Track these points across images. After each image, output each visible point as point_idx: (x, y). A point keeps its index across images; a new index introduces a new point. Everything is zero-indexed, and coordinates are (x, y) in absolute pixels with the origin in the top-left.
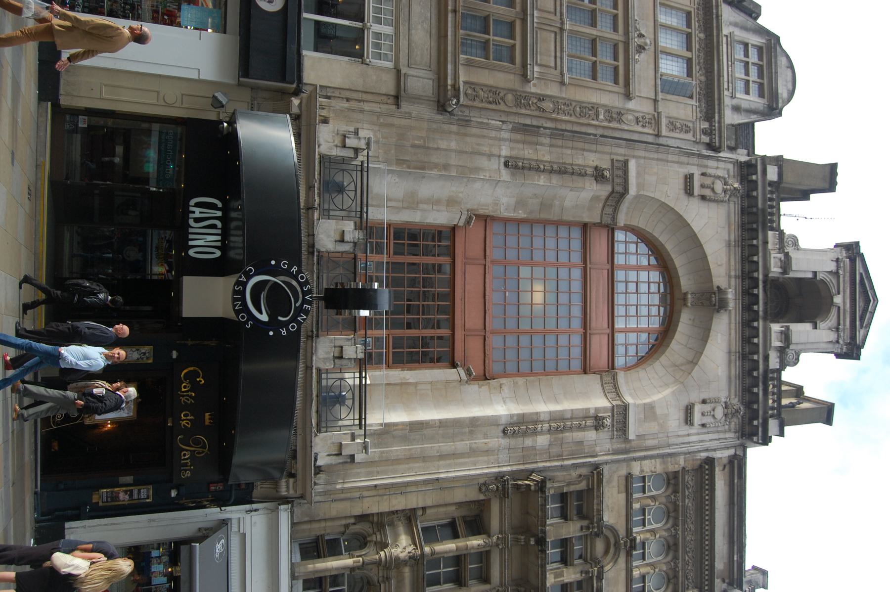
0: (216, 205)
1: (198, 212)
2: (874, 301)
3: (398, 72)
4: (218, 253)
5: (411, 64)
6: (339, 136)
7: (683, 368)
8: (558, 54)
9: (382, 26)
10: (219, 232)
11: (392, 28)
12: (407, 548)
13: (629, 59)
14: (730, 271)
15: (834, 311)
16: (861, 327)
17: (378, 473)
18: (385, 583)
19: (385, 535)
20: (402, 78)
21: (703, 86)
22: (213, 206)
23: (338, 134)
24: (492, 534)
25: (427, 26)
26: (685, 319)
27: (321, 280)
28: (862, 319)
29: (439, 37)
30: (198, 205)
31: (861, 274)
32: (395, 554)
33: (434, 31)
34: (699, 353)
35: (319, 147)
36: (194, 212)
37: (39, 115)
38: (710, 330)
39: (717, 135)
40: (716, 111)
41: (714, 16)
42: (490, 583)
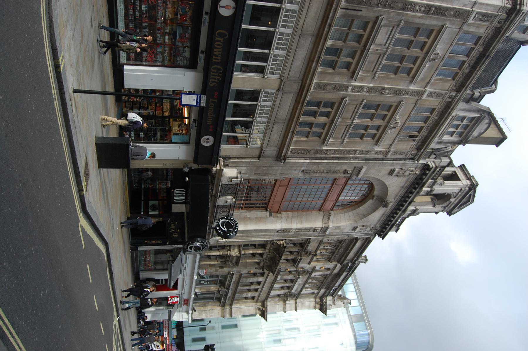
1: (177, 192)
2: (472, 202)
3: (262, 149)
4: (184, 201)
5: (303, 31)
7: (360, 216)
8: (345, 133)
11: (285, 51)
13: (384, 133)
14: (398, 194)
15: (448, 203)
16: (458, 208)
19: (231, 248)
20: (263, 152)
21: (423, 138)
22: (183, 191)
25: (279, 134)
26: (369, 203)
28: (462, 205)
29: (284, 137)
30: (177, 191)
31: (470, 195)
33: (282, 135)
34: (369, 214)
38: (377, 209)
39: (418, 156)
40: (424, 148)
41: (448, 113)
42: (262, 257)
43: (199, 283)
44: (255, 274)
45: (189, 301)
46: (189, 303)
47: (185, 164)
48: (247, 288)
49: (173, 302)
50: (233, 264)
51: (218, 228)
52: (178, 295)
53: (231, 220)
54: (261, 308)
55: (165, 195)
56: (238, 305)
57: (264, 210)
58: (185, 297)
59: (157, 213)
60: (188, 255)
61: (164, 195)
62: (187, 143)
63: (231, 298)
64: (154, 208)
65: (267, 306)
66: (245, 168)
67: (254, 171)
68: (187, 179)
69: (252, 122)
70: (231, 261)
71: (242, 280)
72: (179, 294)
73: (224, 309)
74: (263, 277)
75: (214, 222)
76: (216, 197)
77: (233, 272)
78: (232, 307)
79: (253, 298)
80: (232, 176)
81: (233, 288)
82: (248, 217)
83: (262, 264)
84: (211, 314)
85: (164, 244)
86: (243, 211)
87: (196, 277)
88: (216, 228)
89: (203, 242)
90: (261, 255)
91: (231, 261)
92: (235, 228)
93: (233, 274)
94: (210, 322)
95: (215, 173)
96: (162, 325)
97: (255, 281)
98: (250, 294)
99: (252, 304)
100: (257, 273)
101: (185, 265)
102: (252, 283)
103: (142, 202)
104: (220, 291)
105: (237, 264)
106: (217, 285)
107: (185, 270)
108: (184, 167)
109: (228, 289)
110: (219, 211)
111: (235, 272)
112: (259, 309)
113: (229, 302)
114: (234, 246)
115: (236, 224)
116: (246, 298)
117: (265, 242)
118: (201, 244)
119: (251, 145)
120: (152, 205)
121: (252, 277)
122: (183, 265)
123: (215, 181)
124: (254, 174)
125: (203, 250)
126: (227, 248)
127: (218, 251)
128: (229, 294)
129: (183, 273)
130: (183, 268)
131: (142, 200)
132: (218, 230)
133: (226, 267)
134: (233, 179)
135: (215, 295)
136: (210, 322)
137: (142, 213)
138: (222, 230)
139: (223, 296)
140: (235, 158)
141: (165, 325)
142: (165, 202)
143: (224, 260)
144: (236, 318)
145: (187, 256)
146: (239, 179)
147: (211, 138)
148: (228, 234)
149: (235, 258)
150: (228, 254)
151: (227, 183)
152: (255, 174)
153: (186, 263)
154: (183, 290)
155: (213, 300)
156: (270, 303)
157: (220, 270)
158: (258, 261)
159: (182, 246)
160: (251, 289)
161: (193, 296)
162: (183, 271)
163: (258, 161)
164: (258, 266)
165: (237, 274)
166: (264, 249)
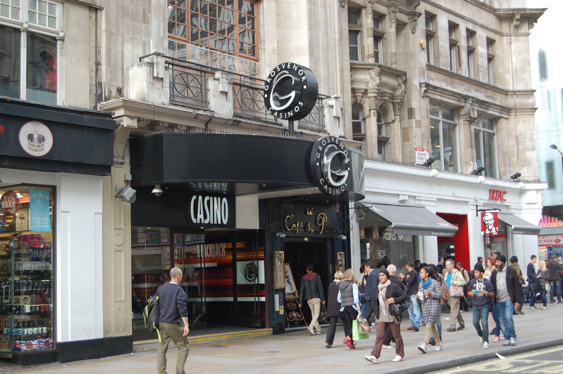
0: (195, 200)
1: (200, 216)
4: (225, 200)
6: (154, 83)
9: (21, 6)
10: (211, 198)
12: (371, 76)
17: (333, 88)
18: (385, 96)
19: (360, 89)
23: (153, 84)
24: (364, 5)
27: (487, 150)
30: (196, 217)
32: (376, 85)
35: (164, 104)
36: (201, 219)
37: (143, 351)
42: (386, 15)
43: (450, 165)
44: (430, 36)
45: (495, 189)
46: (500, 189)
47: (116, 197)
48: (464, 54)
49: (495, 225)
50: (399, 85)
51: (291, 114)
52: (479, 213)
53: (272, 82)
54: (515, 23)
55: (224, 246)
56: (509, 77)
57: (258, 7)
58: (484, 197)
59: (262, 264)
60: (366, 189)
61: (223, 249)
62: (53, 192)
63: (490, 93)
64: (252, 272)
65: (509, 10)
66: (128, 48)
67: (137, 25)
68: (155, 191)
69: (32, 37)
70: (394, 89)
71: (444, 66)
72: (477, 211)
73: (516, 110)
74: (438, 17)
75: (281, 125)
76: (208, 119)
77: (424, 85)
78: (510, 91)
79: (490, 42)
80: (145, 78)
81: (464, 88)
82: (276, 45)
83: (403, 18)
84: (528, 140)
85: (346, 247)
86: (262, 57)
87: (433, 172)
88: (291, 120)
89: (320, 148)
90: (378, 18)
91: (394, 89)
92: (291, 71)
93: (427, 85)
94: (554, 147)
95: (139, 120)
96: (554, 249)
97: (448, 34)
98: (482, 50)
99: (505, 46)
100: (427, 30)
101: (401, 198)
102: (453, 44)
103: (240, 299)
104: (470, 117)
105: (400, 75)
106: (456, 125)
107: (415, 197)
108: (123, 198)
109: (466, 98)
110: (251, 114)
111: (422, 81)
112: (517, 27)
113: (499, 98)
114: (352, 82)
115: (282, 70)
116: (490, 59)
117: (343, 7)
118: (328, 155)
119: (57, 29)
120: (245, 276)
121: (438, 41)
122: (403, 201)
123: (162, 122)
124: (145, 22)
125: (345, 148)
126: (359, 98)
127: (367, 120)
128: (481, 95)
129: (422, 203)
130: (411, 202)
131: (235, 299)
132: (294, 112)
133: (409, 101)
134: (155, 75)
135: (482, 129)
136: (554, 147)
137: (263, 299)
138: (295, 103)
139: (483, 110)
140: (97, 70)
141: (554, 243)
142: (239, 245)
143: (391, 107)
144: (548, 92)
145: (366, 191)
146: (155, 61)
147: (27, 129)
148: (305, 87)
149: (385, 79)
150: (376, 95)
151: (168, 90)
152: (146, 20)
153: (398, 195)
154: (466, 203)
155: (494, 134)
156: (505, 4)
157: (417, 116)
158: (394, 25)
159: (351, 204)
160: (468, 47)
161: (481, 179)
162: (417, 203)
163: (104, 11)
164: (408, 26)
165: (429, 78)
166: (364, 11)
